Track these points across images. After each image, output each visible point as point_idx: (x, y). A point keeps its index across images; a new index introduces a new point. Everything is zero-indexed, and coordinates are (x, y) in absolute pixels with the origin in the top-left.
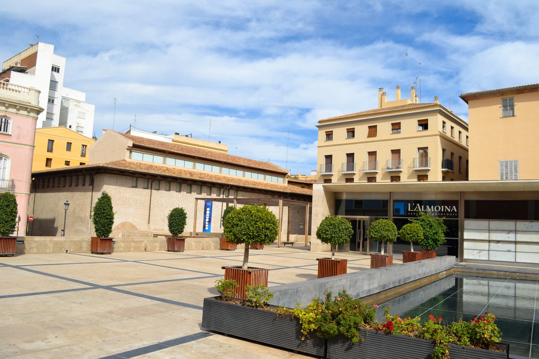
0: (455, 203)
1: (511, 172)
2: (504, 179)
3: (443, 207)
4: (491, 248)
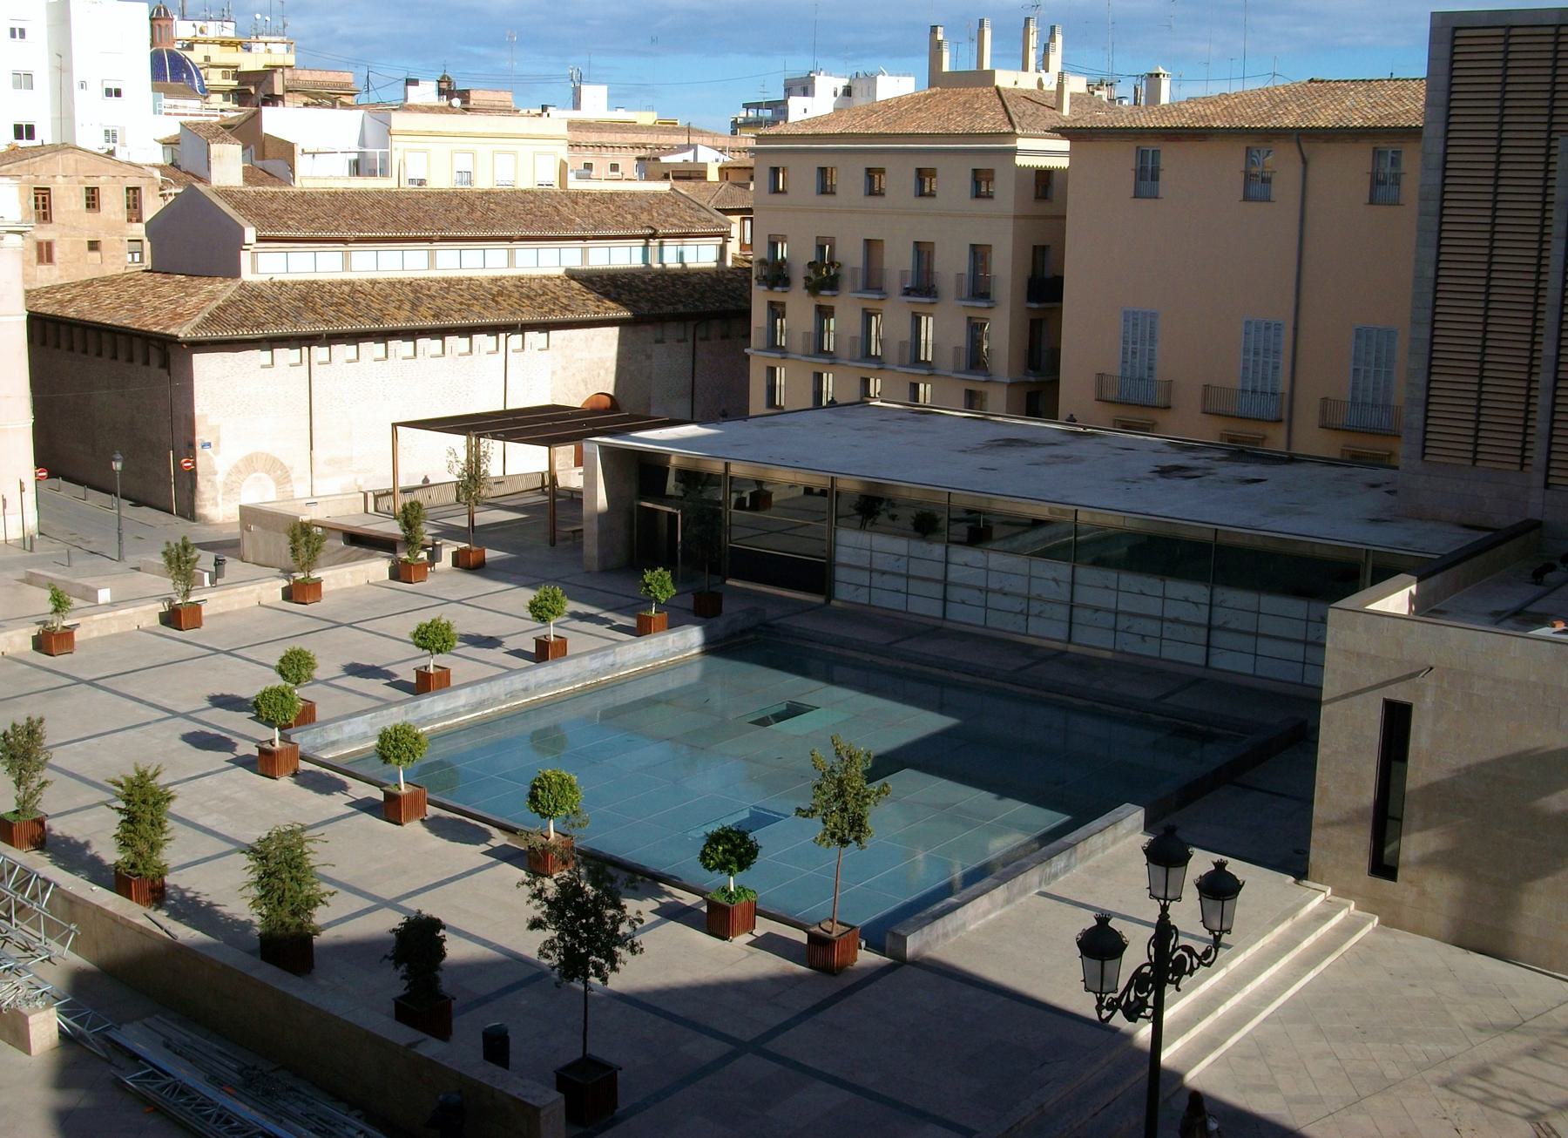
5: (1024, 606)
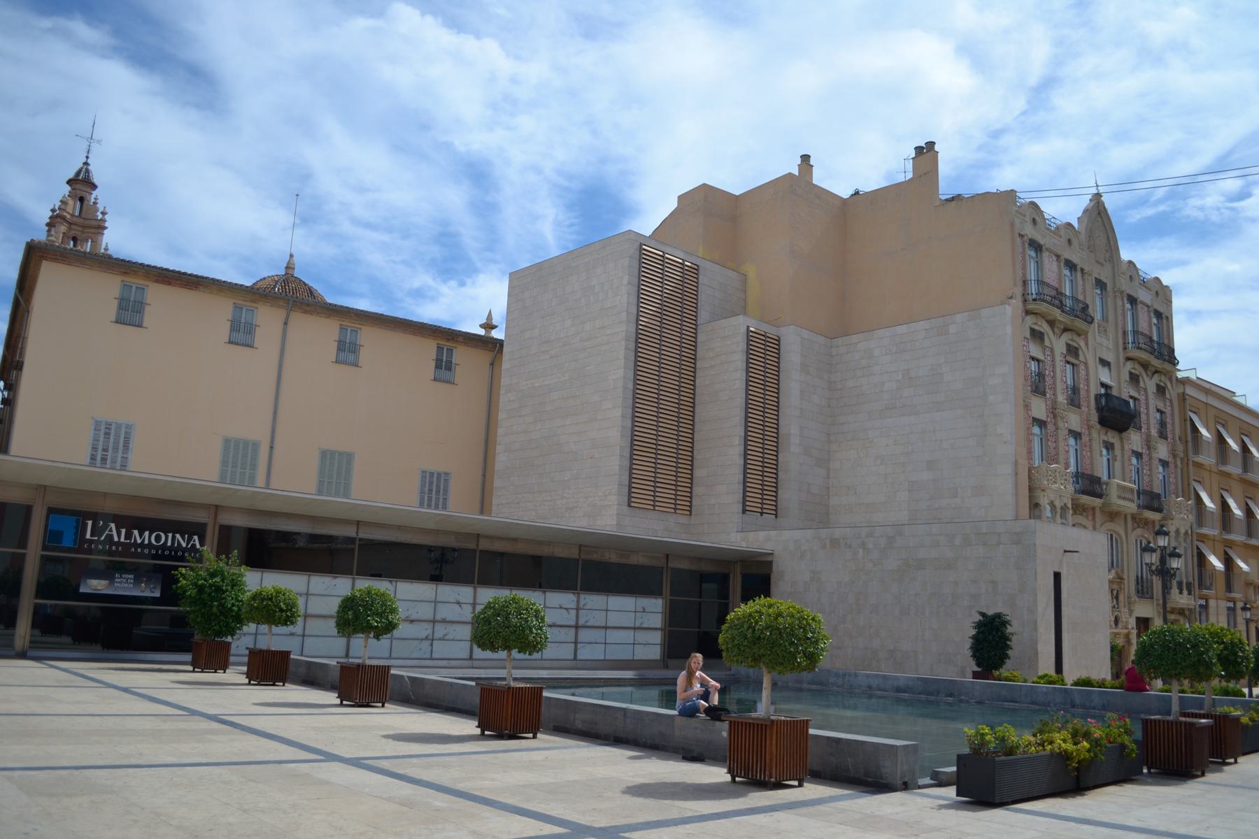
0: (198, 530)
1: (438, 492)
2: (118, 466)
3: (170, 535)
4: (438, 634)
5: (430, 631)
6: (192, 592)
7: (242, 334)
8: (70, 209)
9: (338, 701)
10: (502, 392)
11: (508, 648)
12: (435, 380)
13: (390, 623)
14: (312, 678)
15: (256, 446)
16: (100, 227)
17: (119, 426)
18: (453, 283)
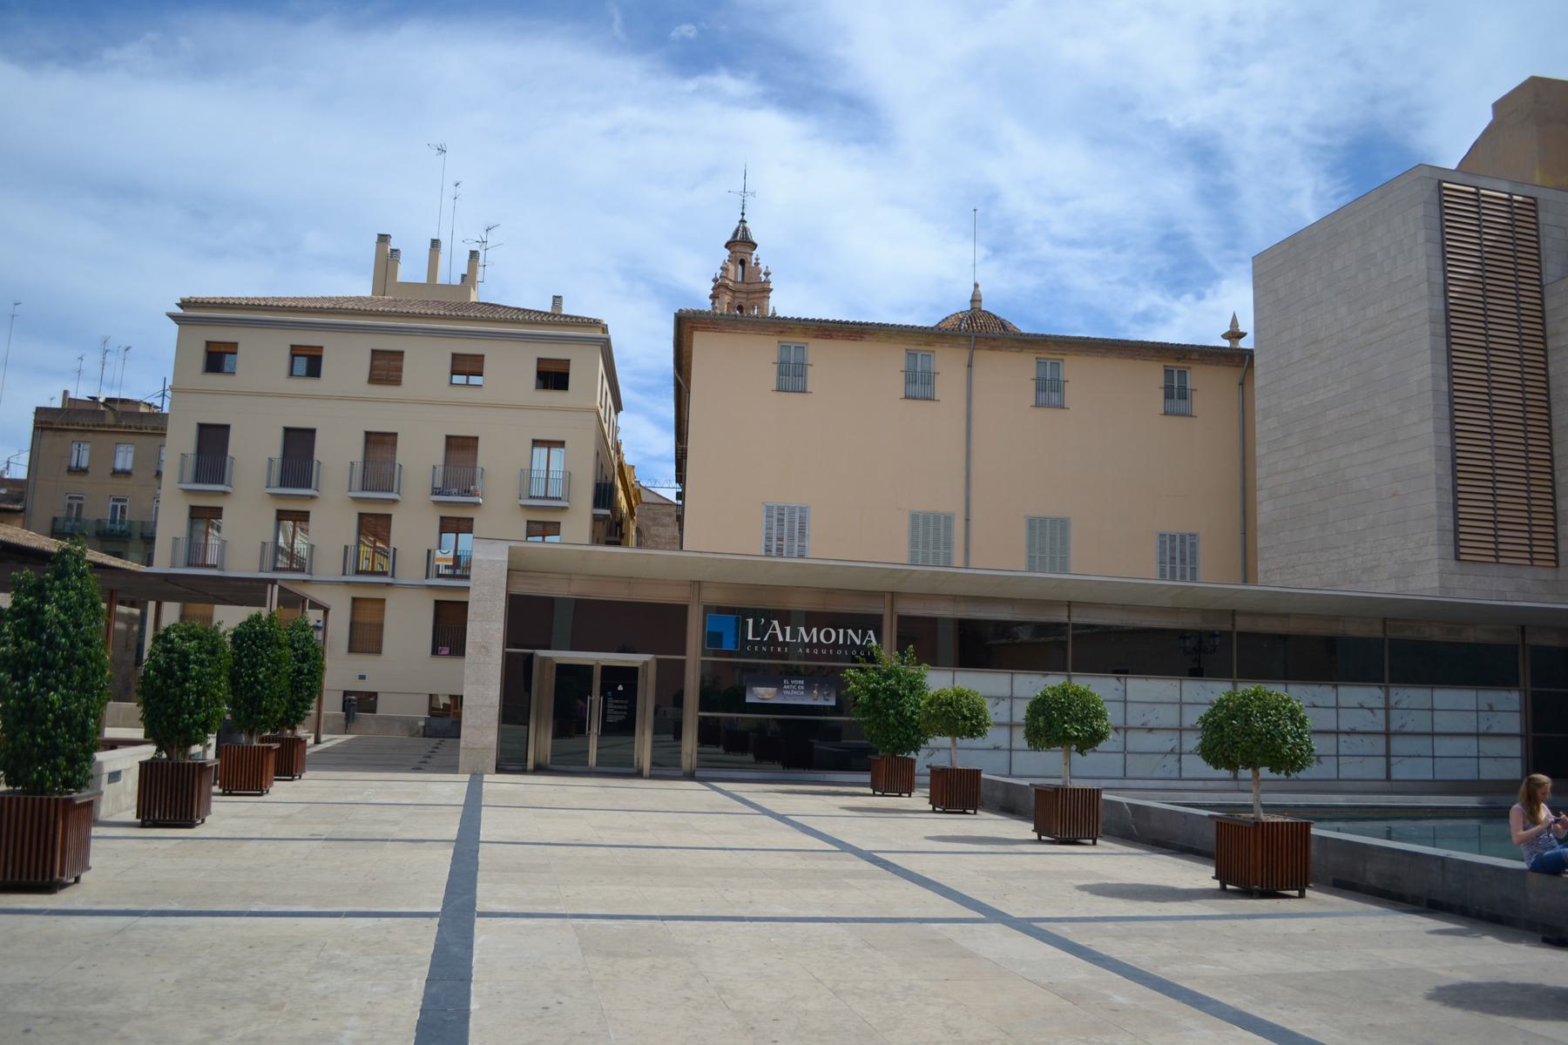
0: (869, 622)
1: (1183, 560)
5: (1175, 742)
6: (864, 698)
7: (919, 386)
8: (731, 275)
9: (1035, 836)
10: (1258, 418)
11: (1252, 764)
12: (1166, 413)
13: (1096, 731)
14: (1008, 805)
15: (949, 518)
16: (766, 291)
17: (792, 511)
18: (1189, 297)
